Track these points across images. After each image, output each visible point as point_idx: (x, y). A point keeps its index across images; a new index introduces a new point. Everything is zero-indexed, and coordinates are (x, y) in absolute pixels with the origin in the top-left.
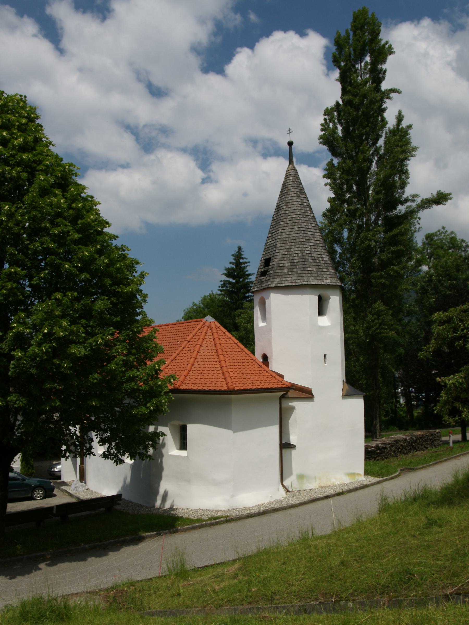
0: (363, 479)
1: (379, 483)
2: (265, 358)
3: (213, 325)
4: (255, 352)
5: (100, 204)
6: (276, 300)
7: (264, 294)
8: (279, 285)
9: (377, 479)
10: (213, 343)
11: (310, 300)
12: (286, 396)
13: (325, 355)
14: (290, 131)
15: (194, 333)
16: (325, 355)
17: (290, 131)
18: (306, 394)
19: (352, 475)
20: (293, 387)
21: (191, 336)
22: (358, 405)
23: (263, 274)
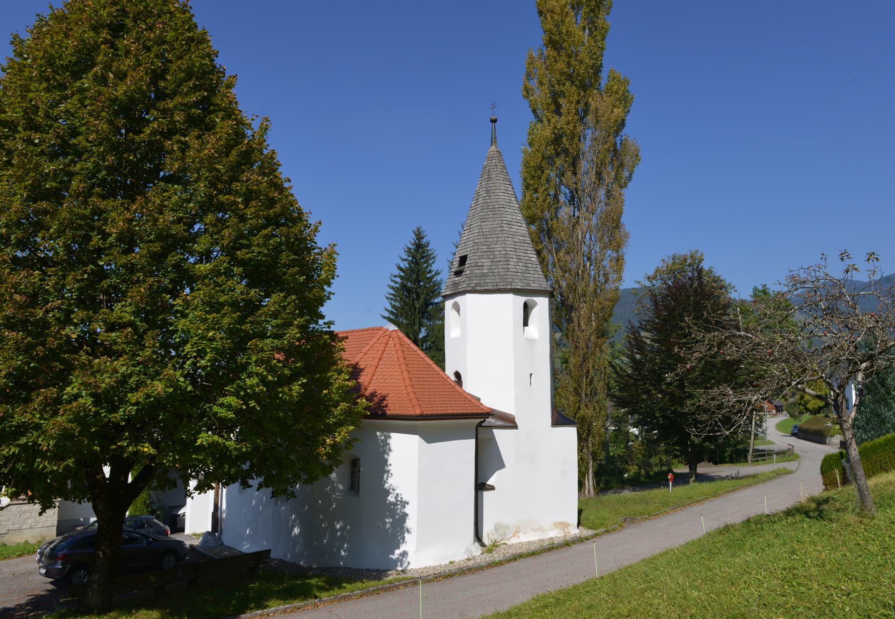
0: (574, 531)
1: (596, 535)
2: (458, 375)
3: (394, 335)
4: (443, 360)
5: (40, 514)
6: (469, 301)
7: (459, 299)
8: (477, 288)
9: (594, 532)
10: (402, 384)
11: (512, 303)
12: (483, 424)
13: (463, 260)
14: (493, 106)
15: (371, 343)
16: (463, 260)
17: (493, 106)
18: (509, 422)
19: (564, 525)
20: (490, 413)
21: (369, 347)
22: (570, 434)
23: (458, 273)
